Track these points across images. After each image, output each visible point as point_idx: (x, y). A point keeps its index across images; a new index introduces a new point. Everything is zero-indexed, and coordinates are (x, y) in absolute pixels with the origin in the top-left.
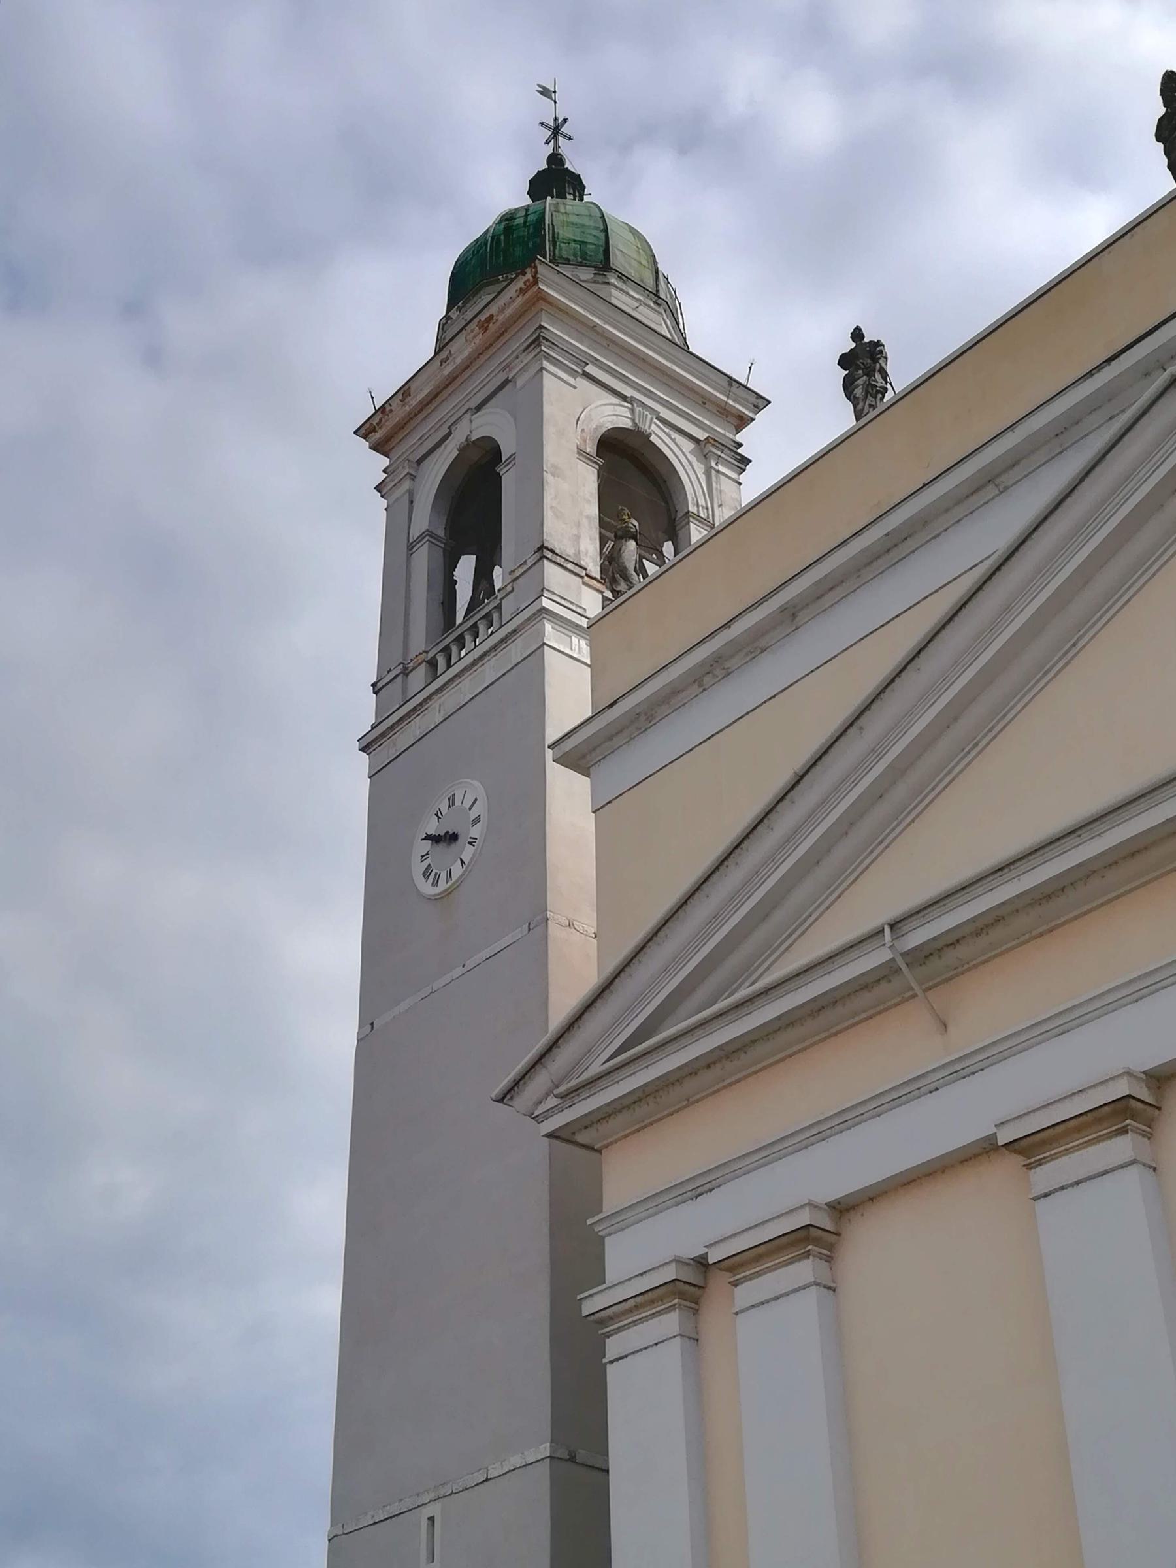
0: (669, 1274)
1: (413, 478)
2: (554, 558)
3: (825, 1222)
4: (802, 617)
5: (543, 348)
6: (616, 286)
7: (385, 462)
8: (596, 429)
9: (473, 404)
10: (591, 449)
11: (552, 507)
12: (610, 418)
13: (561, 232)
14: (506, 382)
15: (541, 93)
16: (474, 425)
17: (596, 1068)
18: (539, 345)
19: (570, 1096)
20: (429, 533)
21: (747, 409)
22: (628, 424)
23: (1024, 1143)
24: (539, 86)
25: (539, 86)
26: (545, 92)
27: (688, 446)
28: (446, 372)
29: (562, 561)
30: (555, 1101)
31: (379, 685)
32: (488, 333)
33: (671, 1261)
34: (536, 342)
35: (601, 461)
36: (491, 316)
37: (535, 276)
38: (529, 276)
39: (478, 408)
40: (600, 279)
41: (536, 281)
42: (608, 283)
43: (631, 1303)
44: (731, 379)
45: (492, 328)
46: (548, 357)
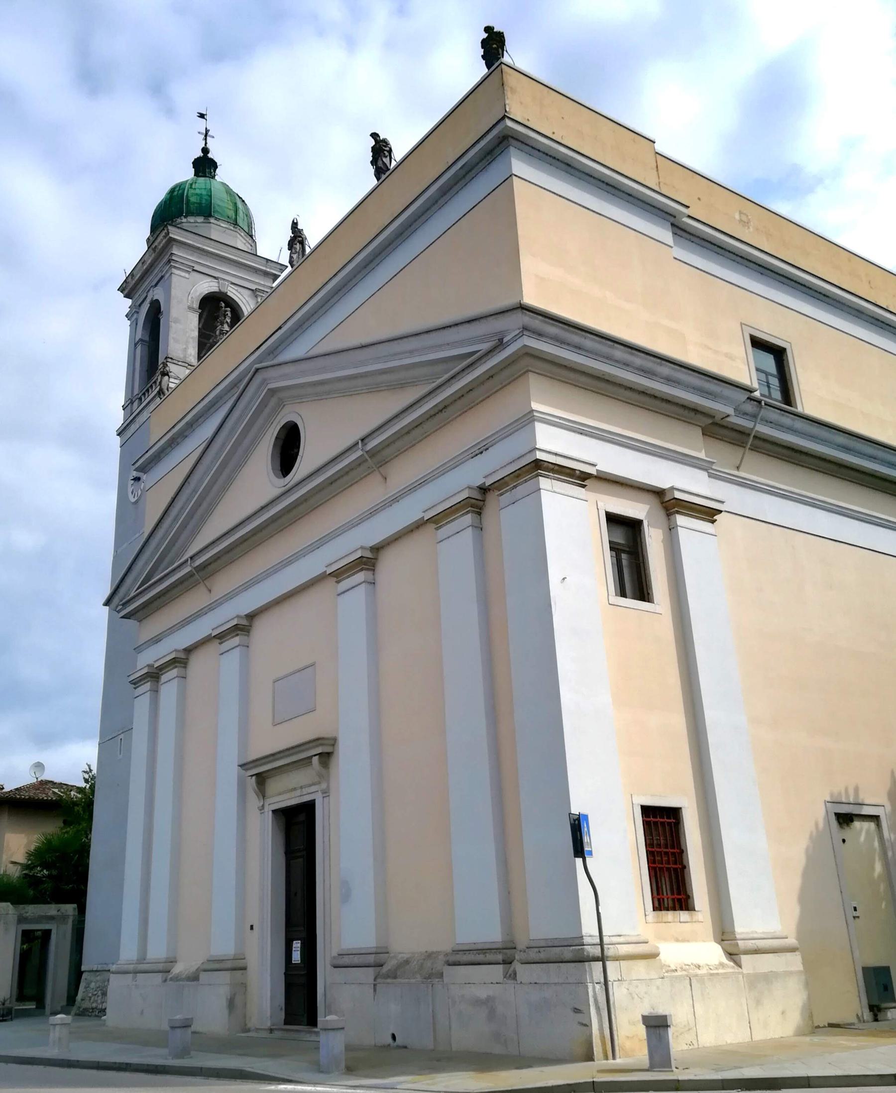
0: (465, 495)
1: (138, 313)
2: (172, 361)
3: (182, 656)
4: (194, 426)
5: (172, 264)
6: (213, 223)
7: (129, 302)
8: (200, 294)
9: (154, 283)
10: (196, 305)
11: (173, 338)
12: (206, 289)
13: (191, 199)
14: (162, 277)
15: (199, 116)
16: (155, 292)
17: (132, 594)
18: (170, 263)
19: (125, 605)
20: (141, 340)
21: (277, 271)
22: (216, 289)
23: (220, 635)
24: (198, 113)
25: (198, 113)
26: (202, 116)
27: (246, 293)
28: (145, 267)
29: (176, 362)
30: (121, 607)
31: (125, 407)
32: (156, 252)
33: (466, 488)
34: (169, 261)
35: (200, 311)
36: (156, 246)
37: (168, 230)
38: (166, 231)
39: (156, 285)
40: (206, 221)
41: (168, 233)
42: (210, 223)
43: (140, 678)
44: (268, 260)
45: (157, 251)
46: (175, 267)
